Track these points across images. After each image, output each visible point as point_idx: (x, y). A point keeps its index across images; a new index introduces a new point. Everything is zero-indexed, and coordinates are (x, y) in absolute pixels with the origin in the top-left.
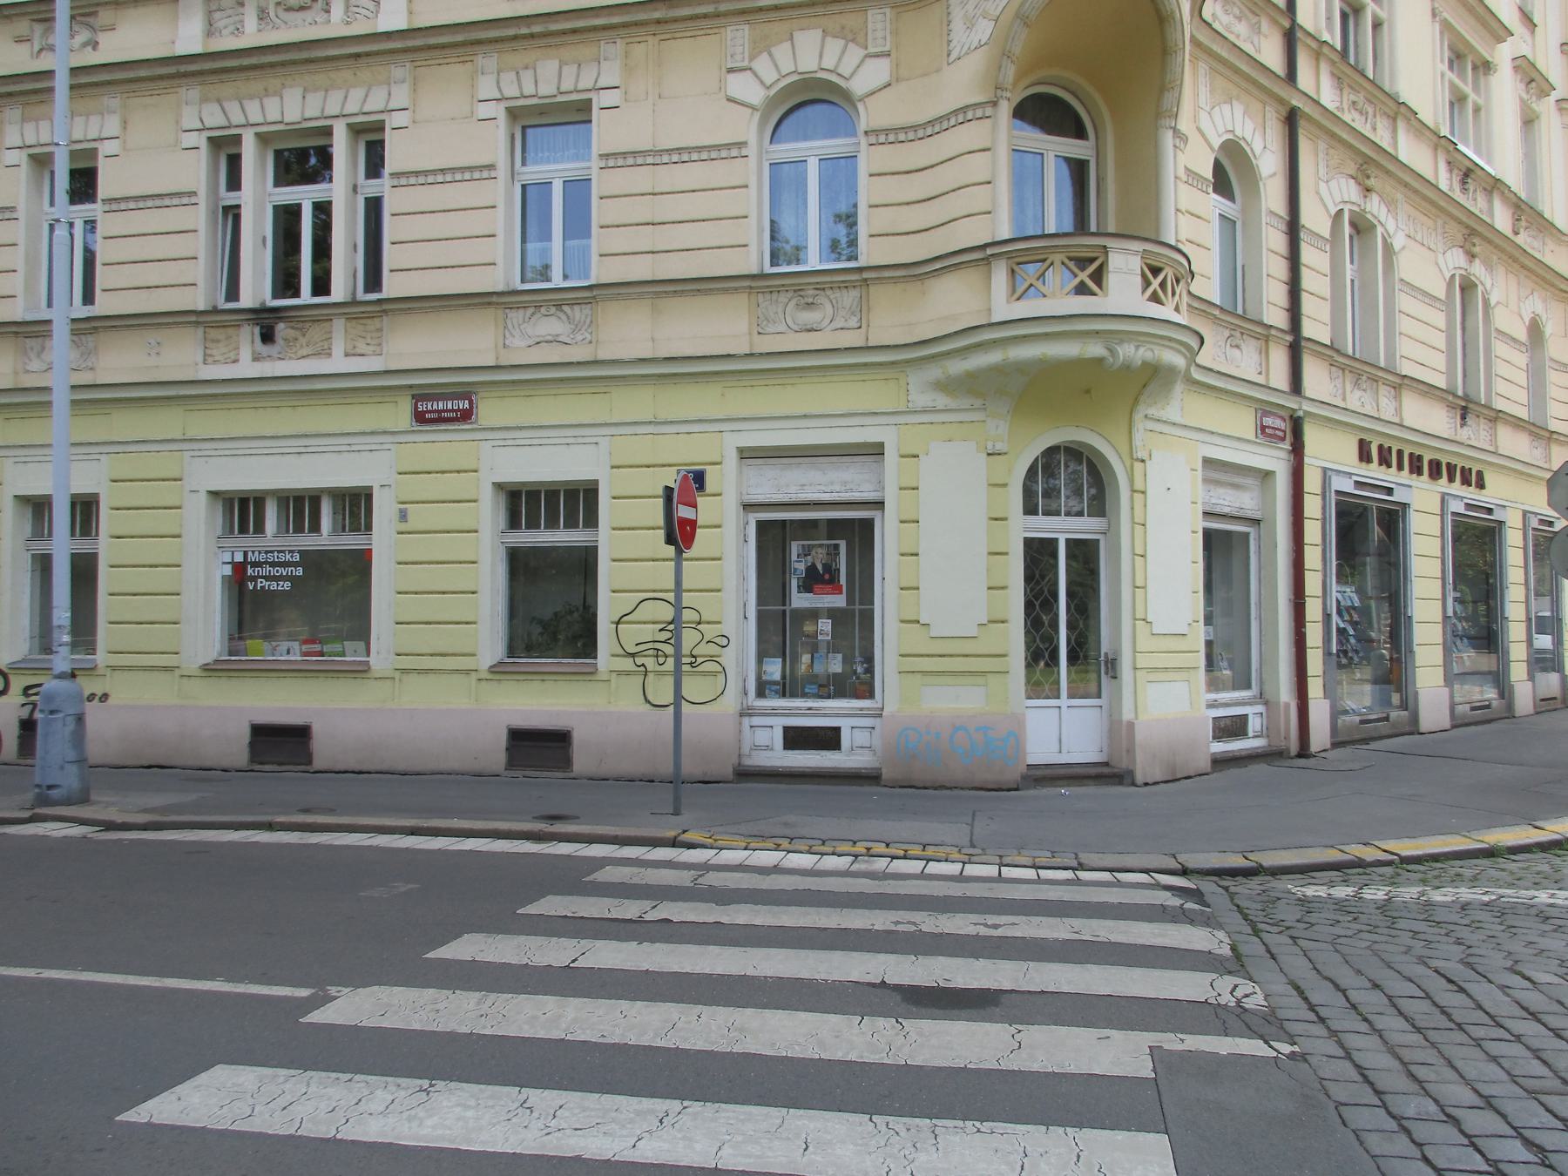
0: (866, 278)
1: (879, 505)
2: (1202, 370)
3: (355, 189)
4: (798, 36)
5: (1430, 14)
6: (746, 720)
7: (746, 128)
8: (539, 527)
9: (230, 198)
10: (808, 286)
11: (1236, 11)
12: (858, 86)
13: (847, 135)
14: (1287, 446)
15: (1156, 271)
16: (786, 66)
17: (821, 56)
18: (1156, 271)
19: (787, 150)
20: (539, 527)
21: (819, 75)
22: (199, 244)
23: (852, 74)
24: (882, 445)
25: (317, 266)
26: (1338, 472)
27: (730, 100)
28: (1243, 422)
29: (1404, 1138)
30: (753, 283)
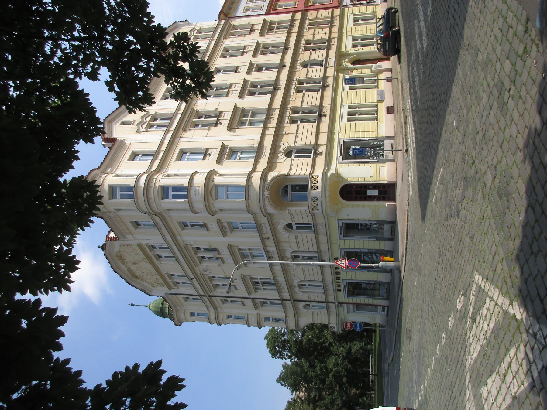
7: (293, 235)
9: (301, 257)
22: (311, 93)
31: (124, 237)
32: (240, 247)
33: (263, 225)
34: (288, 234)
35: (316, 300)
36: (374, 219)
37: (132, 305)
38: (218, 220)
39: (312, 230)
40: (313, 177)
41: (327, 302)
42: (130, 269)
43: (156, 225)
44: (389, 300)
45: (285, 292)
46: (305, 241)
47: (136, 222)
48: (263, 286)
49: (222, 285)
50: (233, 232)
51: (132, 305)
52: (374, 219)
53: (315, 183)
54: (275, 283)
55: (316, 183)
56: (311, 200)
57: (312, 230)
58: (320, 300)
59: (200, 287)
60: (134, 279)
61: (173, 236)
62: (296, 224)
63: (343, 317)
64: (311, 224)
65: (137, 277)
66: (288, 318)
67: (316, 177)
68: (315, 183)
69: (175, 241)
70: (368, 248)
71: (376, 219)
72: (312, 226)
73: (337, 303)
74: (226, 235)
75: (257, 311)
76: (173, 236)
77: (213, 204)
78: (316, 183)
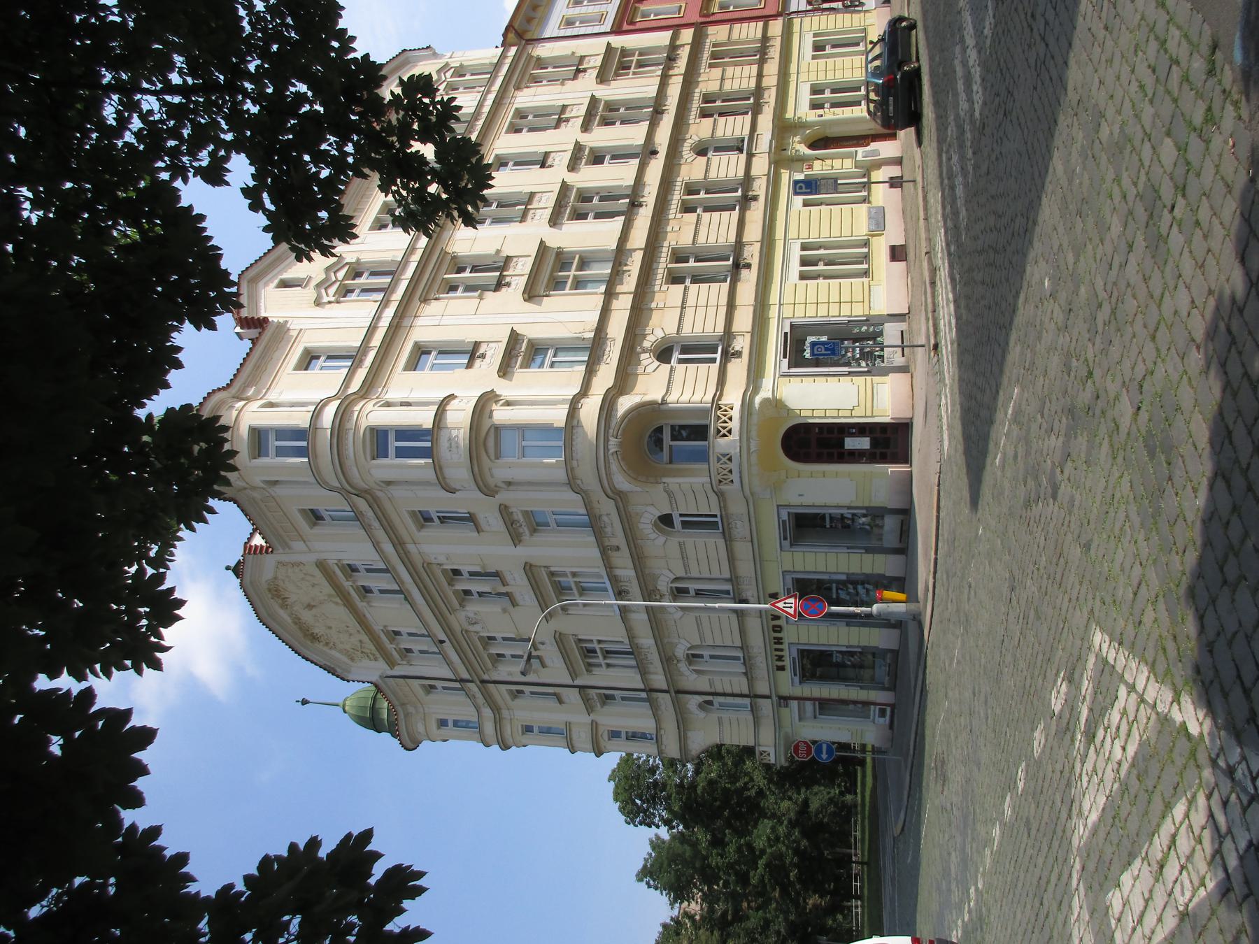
7: (673, 542)
9: (692, 593)
22: (716, 215)
31: (286, 546)
32: (553, 569)
33: (605, 518)
34: (662, 539)
35: (728, 690)
36: (860, 505)
37: (305, 702)
38: (502, 507)
39: (718, 529)
40: (720, 408)
41: (754, 696)
42: (300, 619)
43: (358, 517)
44: (895, 691)
45: (656, 673)
46: (702, 555)
47: (312, 511)
48: (605, 658)
49: (510, 657)
50: (535, 534)
51: (305, 702)
52: (861, 505)
53: (725, 422)
54: (634, 651)
55: (728, 420)
56: (716, 461)
57: (718, 529)
58: (737, 691)
59: (460, 661)
60: (309, 643)
61: (399, 544)
62: (681, 515)
63: (789, 730)
64: (715, 516)
65: (315, 638)
66: (662, 732)
67: (727, 408)
68: (725, 422)
69: (403, 555)
70: (846, 571)
71: (866, 504)
72: (718, 519)
73: (775, 698)
74: (520, 541)
75: (592, 716)
76: (399, 544)
77: (490, 469)
78: (728, 420)
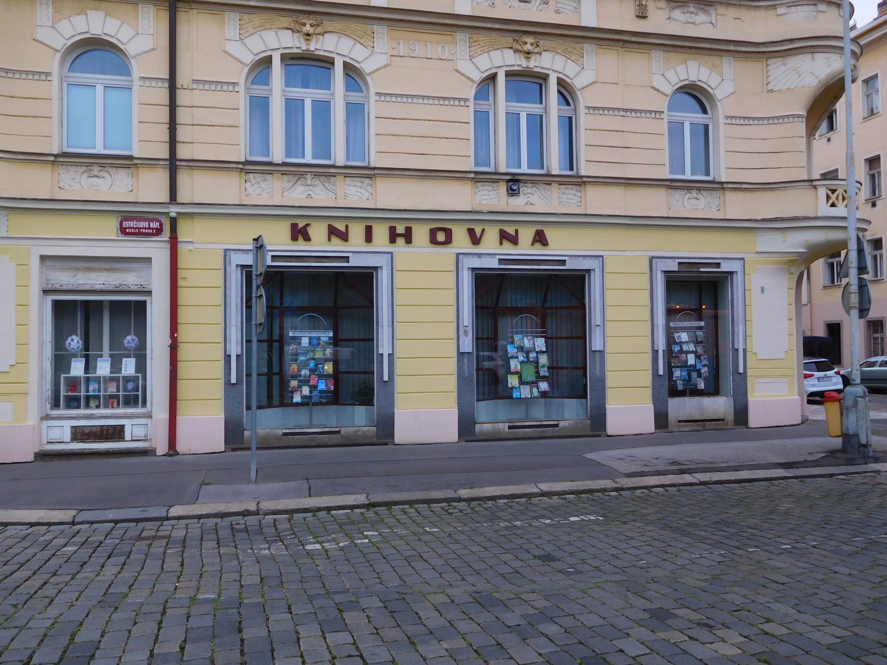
0: (581, 182)
1: (149, 293)
2: (3, 200)
3: (575, 110)
4: (688, 62)
5: (852, 105)
6: (45, 423)
7: (662, 104)
8: (110, 351)
10: (268, 168)
11: (692, 9)
12: (131, 49)
13: (485, 100)
14: (166, 235)
15: (834, 191)
16: (683, 76)
17: (350, 51)
18: (834, 191)
19: (97, 79)
20: (110, 351)
21: (697, 83)
23: (126, 43)
24: (150, 258)
25: (699, 173)
26: (233, 250)
27: (457, 71)
28: (109, 227)
29: (379, 554)
30: (246, 167)
